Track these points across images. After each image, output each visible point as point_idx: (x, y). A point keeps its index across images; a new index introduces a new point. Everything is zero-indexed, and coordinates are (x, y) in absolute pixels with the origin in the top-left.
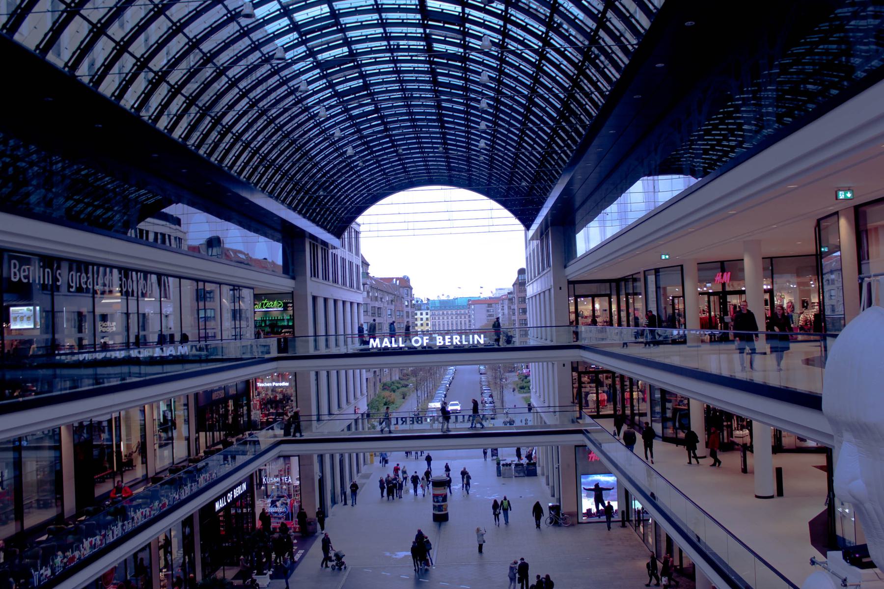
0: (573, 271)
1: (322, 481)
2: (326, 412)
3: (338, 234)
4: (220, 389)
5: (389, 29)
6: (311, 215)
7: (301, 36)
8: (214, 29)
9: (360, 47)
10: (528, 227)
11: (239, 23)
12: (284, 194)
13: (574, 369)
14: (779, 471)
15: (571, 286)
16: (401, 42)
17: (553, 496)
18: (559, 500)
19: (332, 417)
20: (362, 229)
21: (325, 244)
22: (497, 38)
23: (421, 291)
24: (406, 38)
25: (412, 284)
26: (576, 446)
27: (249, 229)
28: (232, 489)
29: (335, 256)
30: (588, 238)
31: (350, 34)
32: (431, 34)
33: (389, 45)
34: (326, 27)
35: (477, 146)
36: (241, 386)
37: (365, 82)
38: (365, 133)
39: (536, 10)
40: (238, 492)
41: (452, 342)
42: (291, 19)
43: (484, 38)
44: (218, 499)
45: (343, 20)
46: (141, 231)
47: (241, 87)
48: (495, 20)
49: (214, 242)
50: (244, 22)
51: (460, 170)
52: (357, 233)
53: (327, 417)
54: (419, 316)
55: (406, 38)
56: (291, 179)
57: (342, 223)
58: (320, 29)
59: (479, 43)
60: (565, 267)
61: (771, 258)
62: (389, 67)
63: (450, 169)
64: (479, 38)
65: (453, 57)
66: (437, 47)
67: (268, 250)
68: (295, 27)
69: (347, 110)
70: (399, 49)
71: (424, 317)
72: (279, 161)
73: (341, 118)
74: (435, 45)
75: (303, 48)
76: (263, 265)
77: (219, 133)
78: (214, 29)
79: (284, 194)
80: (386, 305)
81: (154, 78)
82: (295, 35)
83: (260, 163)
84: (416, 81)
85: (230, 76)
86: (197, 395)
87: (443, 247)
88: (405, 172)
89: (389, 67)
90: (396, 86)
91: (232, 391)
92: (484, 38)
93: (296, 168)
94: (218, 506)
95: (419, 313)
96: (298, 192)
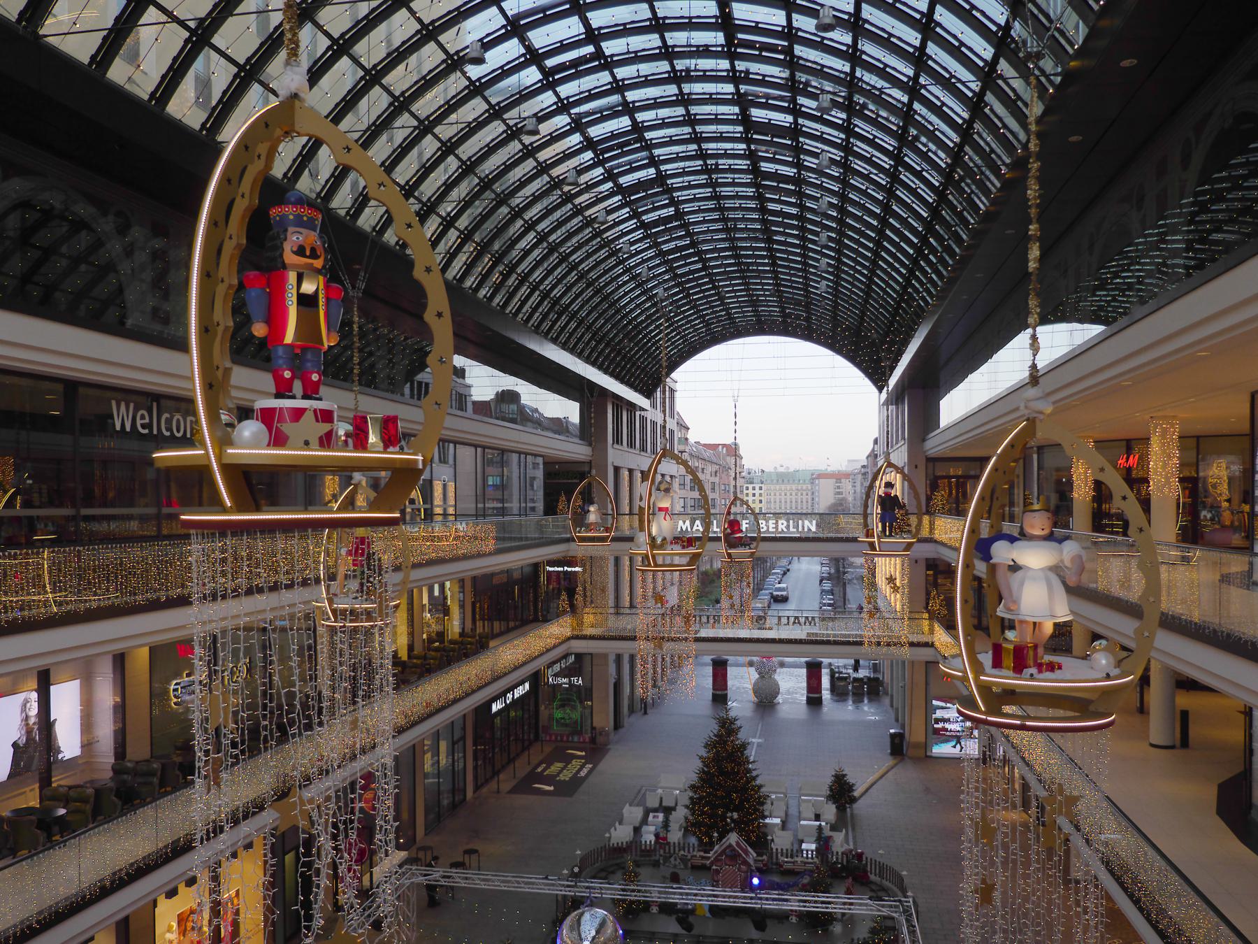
0: (935, 444)
1: (618, 686)
2: (627, 604)
3: (648, 394)
4: (502, 572)
5: (704, 146)
6: (614, 370)
7: (597, 155)
8: (491, 150)
9: (687, 207)
10: (880, 389)
11: (520, 141)
12: (580, 346)
13: (928, 567)
14: (1185, 715)
15: (931, 465)
16: (720, 162)
17: (897, 720)
18: (903, 727)
19: (633, 611)
20: (678, 387)
21: (632, 407)
22: (837, 155)
23: (751, 461)
24: (726, 155)
25: (742, 452)
26: (927, 663)
27: (540, 385)
28: (512, 689)
29: (643, 419)
30: (957, 404)
31: (656, 152)
32: (756, 150)
33: (706, 165)
34: (628, 143)
35: (817, 288)
36: (527, 570)
37: (677, 210)
38: (665, 247)
39: (886, 119)
40: (519, 692)
41: (777, 528)
42: (633, 119)
43: (822, 156)
44: (494, 699)
45: (649, 135)
46: (420, 383)
47: (527, 218)
48: (835, 133)
49: (508, 397)
50: (527, 139)
51: (798, 317)
52: (672, 391)
53: (628, 611)
54: (750, 491)
55: (726, 155)
56: (589, 327)
57: (651, 380)
58: (621, 145)
59: (816, 161)
60: (924, 440)
61: (1198, 437)
62: (707, 192)
63: (785, 316)
64: (816, 155)
65: (786, 179)
66: (766, 167)
67: (568, 410)
68: (589, 144)
69: (657, 245)
70: (717, 170)
71: (757, 492)
72: (575, 307)
73: (651, 253)
74: (762, 164)
75: (600, 170)
76: (558, 426)
77: (501, 273)
78: (491, 150)
79: (580, 346)
80: (708, 477)
81: (421, 209)
82: (589, 155)
83: (550, 309)
84: (704, 222)
85: (462, 228)
86: (474, 579)
87: (779, 411)
88: (730, 318)
89: (707, 192)
90: (715, 216)
91: (517, 575)
92: (822, 156)
93: (595, 315)
94: (496, 707)
95: (750, 486)
96: (598, 343)
